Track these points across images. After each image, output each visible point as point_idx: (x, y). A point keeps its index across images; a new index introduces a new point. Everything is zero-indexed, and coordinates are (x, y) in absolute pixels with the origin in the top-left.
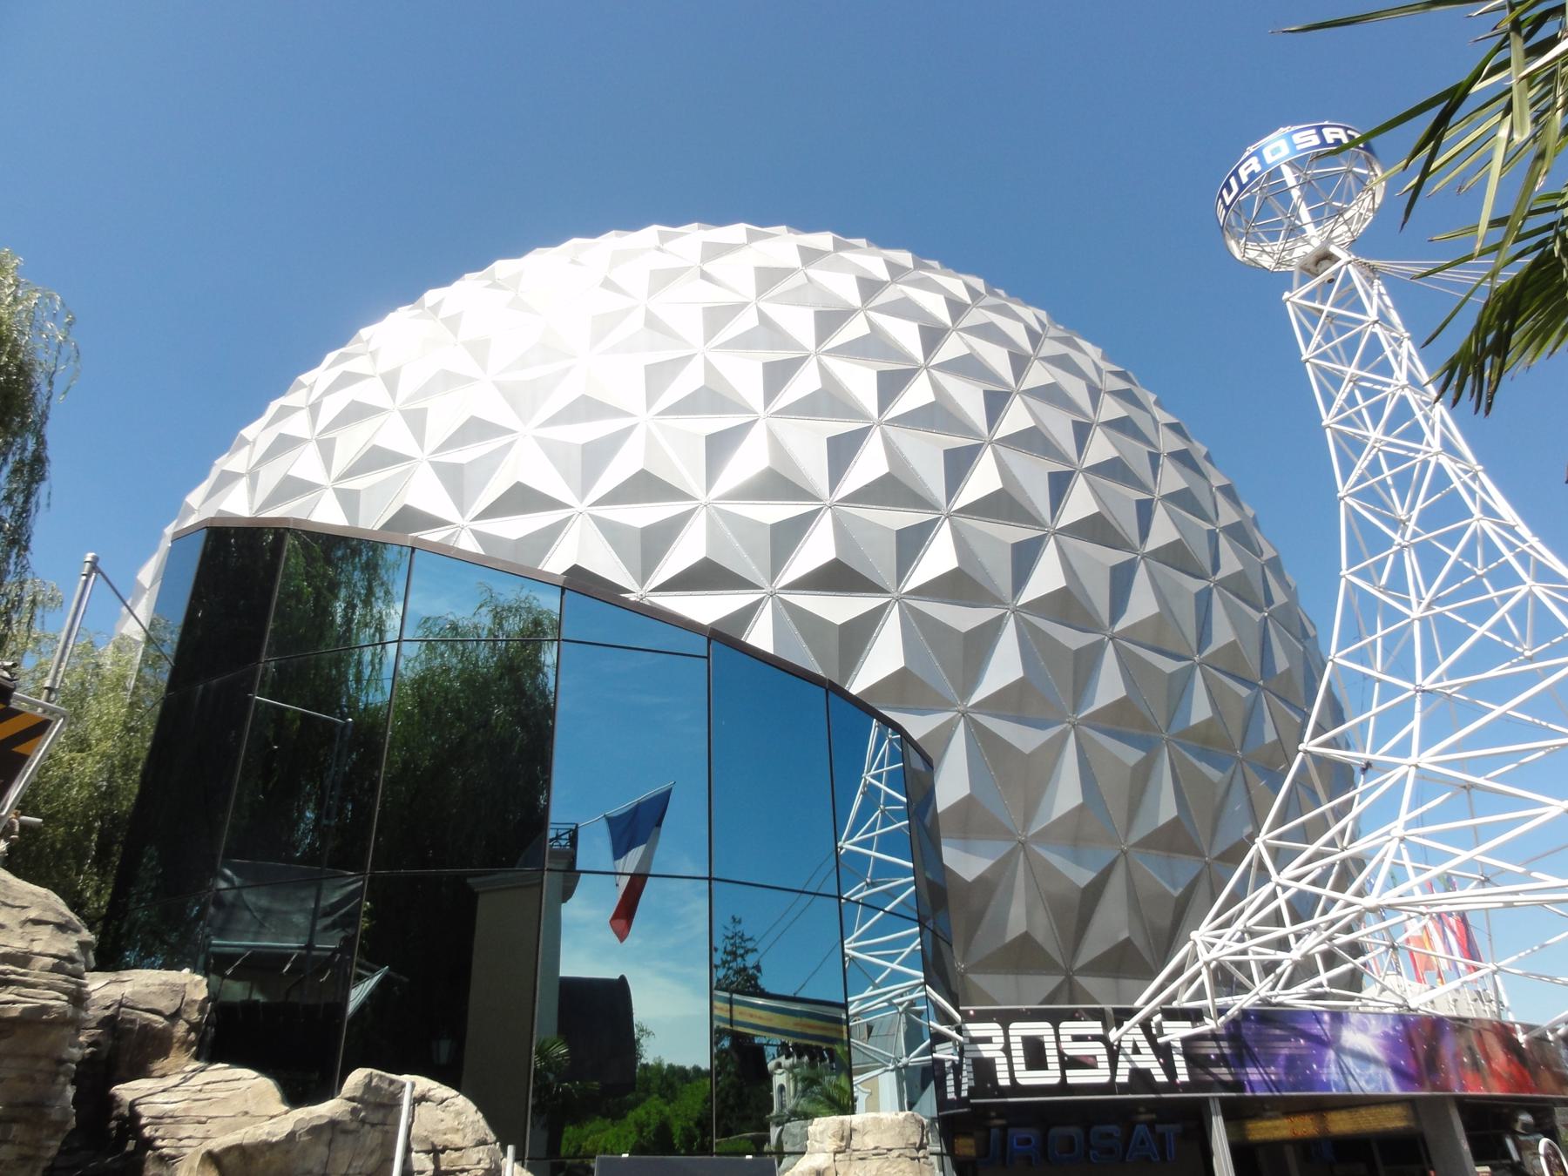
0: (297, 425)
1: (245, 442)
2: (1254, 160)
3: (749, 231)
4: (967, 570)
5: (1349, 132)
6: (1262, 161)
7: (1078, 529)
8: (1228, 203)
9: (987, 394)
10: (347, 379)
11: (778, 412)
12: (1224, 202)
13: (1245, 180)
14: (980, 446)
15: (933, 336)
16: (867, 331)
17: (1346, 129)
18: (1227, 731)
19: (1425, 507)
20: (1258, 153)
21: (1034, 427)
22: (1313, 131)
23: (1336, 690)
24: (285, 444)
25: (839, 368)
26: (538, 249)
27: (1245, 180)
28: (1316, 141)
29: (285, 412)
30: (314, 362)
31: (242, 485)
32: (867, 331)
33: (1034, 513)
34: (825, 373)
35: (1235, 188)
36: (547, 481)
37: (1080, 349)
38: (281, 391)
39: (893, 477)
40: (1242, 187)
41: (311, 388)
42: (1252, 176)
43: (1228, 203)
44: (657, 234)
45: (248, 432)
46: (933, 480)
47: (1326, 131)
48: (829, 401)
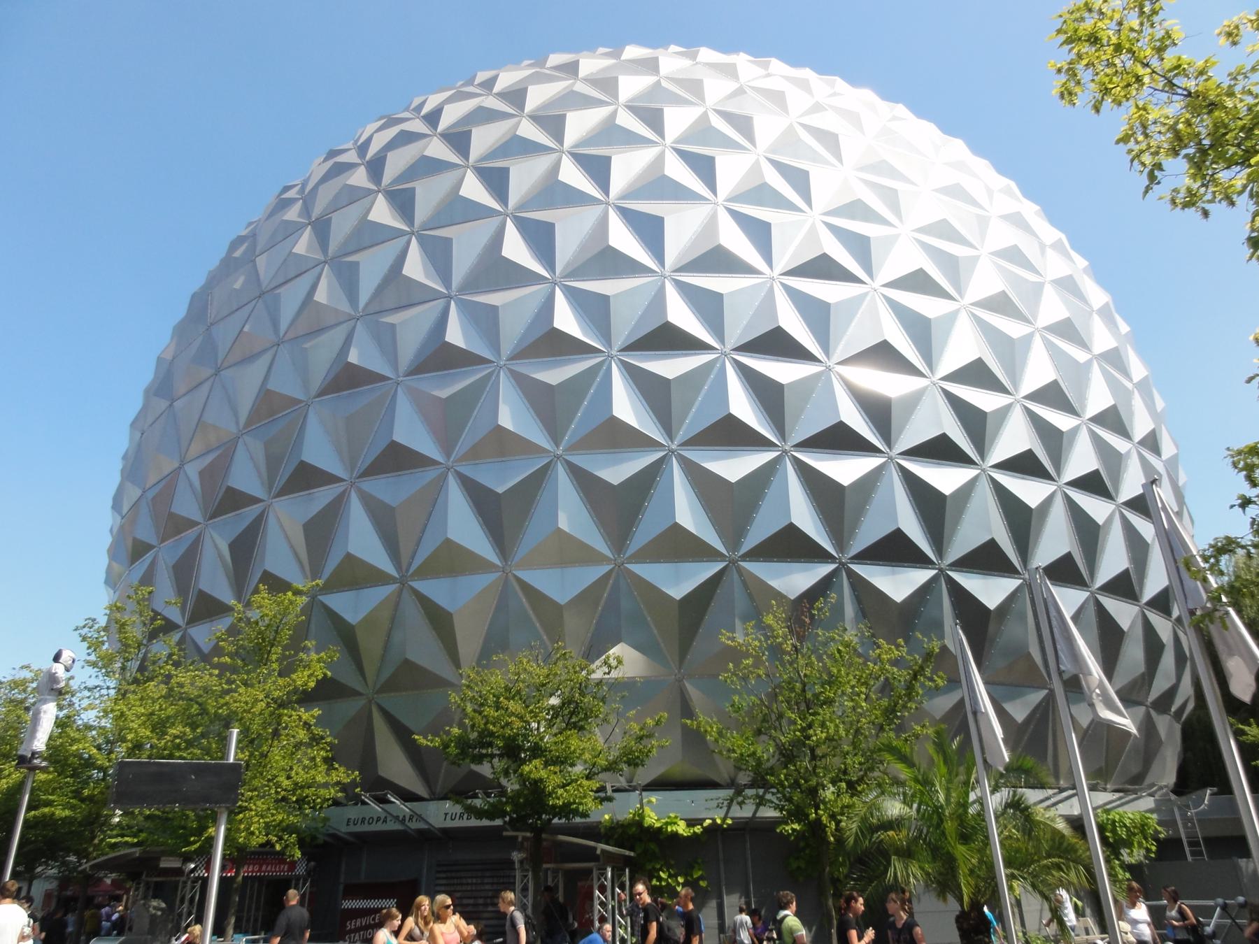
0: (797, 101)
1: (766, 66)
10: (853, 118)
11: (974, 315)
15: (1124, 586)
18: (164, 411)
19: (815, 933)
21: (1099, 526)
23: (392, 805)
24: (778, 99)
25: (1058, 516)
29: (804, 85)
30: (854, 81)
31: (729, 86)
34: (1047, 503)
37: (1190, 649)
38: (822, 70)
39: (930, 325)
41: (835, 94)
44: (1104, 302)
45: (776, 65)
48: (1012, 351)
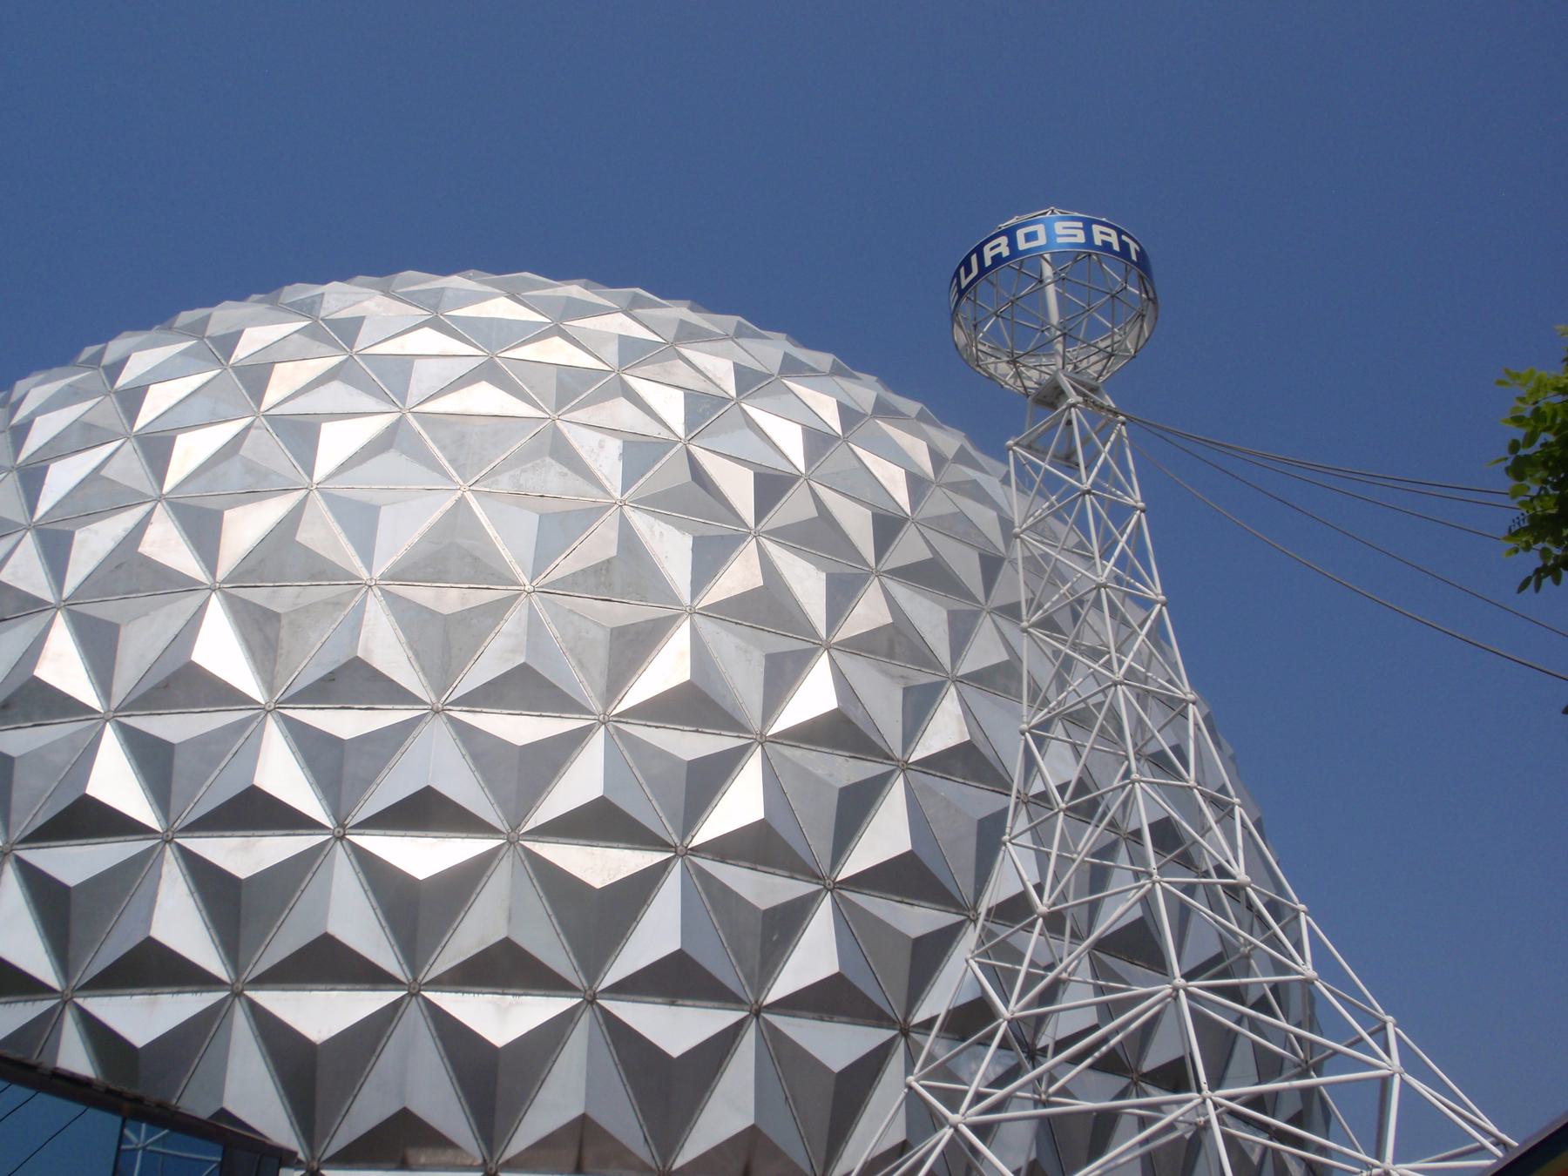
2: (1003, 240)
3: (962, 448)
4: (916, 852)
5: (1124, 238)
6: (1012, 244)
7: (940, 763)
8: (963, 286)
9: (952, 615)
12: (959, 283)
13: (988, 262)
14: (941, 685)
16: (812, 512)
17: (1120, 233)
20: (1010, 233)
22: (1080, 225)
26: (227, 303)
27: (988, 262)
28: (1081, 238)
32: (812, 512)
33: (726, 705)
35: (975, 271)
36: (463, 787)
40: (983, 270)
42: (997, 259)
43: (963, 286)
46: (890, 727)
47: (1096, 229)
